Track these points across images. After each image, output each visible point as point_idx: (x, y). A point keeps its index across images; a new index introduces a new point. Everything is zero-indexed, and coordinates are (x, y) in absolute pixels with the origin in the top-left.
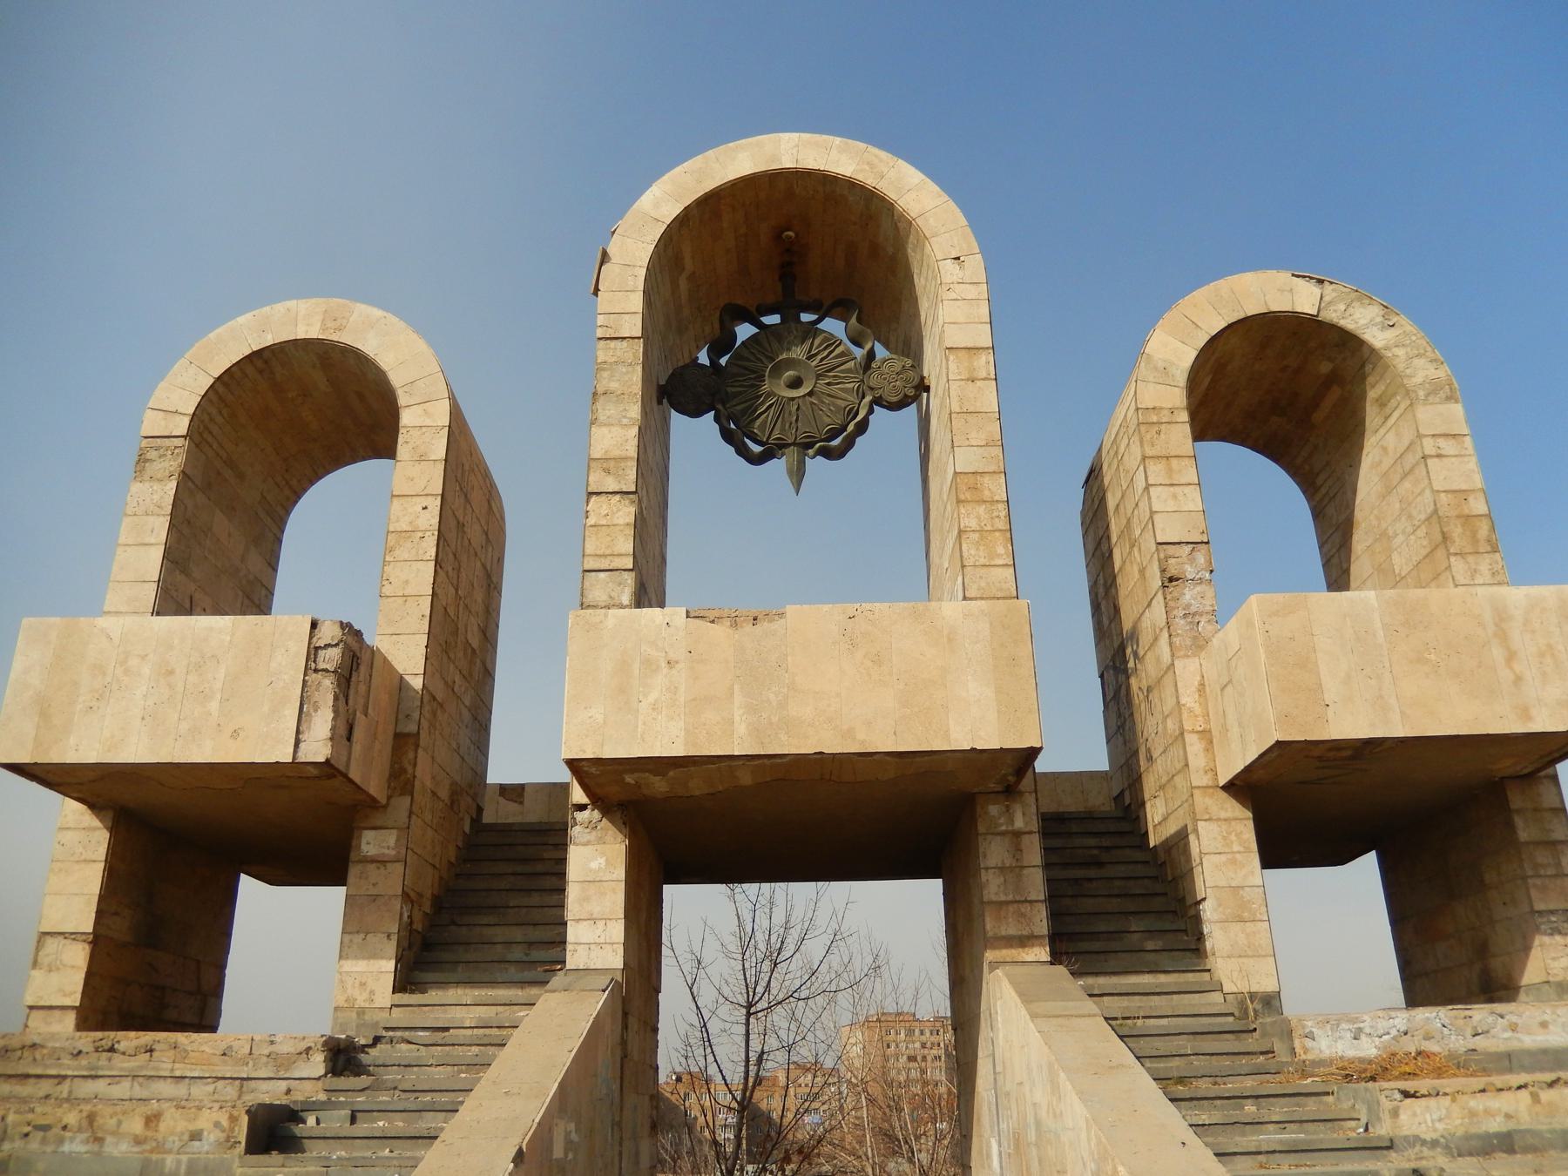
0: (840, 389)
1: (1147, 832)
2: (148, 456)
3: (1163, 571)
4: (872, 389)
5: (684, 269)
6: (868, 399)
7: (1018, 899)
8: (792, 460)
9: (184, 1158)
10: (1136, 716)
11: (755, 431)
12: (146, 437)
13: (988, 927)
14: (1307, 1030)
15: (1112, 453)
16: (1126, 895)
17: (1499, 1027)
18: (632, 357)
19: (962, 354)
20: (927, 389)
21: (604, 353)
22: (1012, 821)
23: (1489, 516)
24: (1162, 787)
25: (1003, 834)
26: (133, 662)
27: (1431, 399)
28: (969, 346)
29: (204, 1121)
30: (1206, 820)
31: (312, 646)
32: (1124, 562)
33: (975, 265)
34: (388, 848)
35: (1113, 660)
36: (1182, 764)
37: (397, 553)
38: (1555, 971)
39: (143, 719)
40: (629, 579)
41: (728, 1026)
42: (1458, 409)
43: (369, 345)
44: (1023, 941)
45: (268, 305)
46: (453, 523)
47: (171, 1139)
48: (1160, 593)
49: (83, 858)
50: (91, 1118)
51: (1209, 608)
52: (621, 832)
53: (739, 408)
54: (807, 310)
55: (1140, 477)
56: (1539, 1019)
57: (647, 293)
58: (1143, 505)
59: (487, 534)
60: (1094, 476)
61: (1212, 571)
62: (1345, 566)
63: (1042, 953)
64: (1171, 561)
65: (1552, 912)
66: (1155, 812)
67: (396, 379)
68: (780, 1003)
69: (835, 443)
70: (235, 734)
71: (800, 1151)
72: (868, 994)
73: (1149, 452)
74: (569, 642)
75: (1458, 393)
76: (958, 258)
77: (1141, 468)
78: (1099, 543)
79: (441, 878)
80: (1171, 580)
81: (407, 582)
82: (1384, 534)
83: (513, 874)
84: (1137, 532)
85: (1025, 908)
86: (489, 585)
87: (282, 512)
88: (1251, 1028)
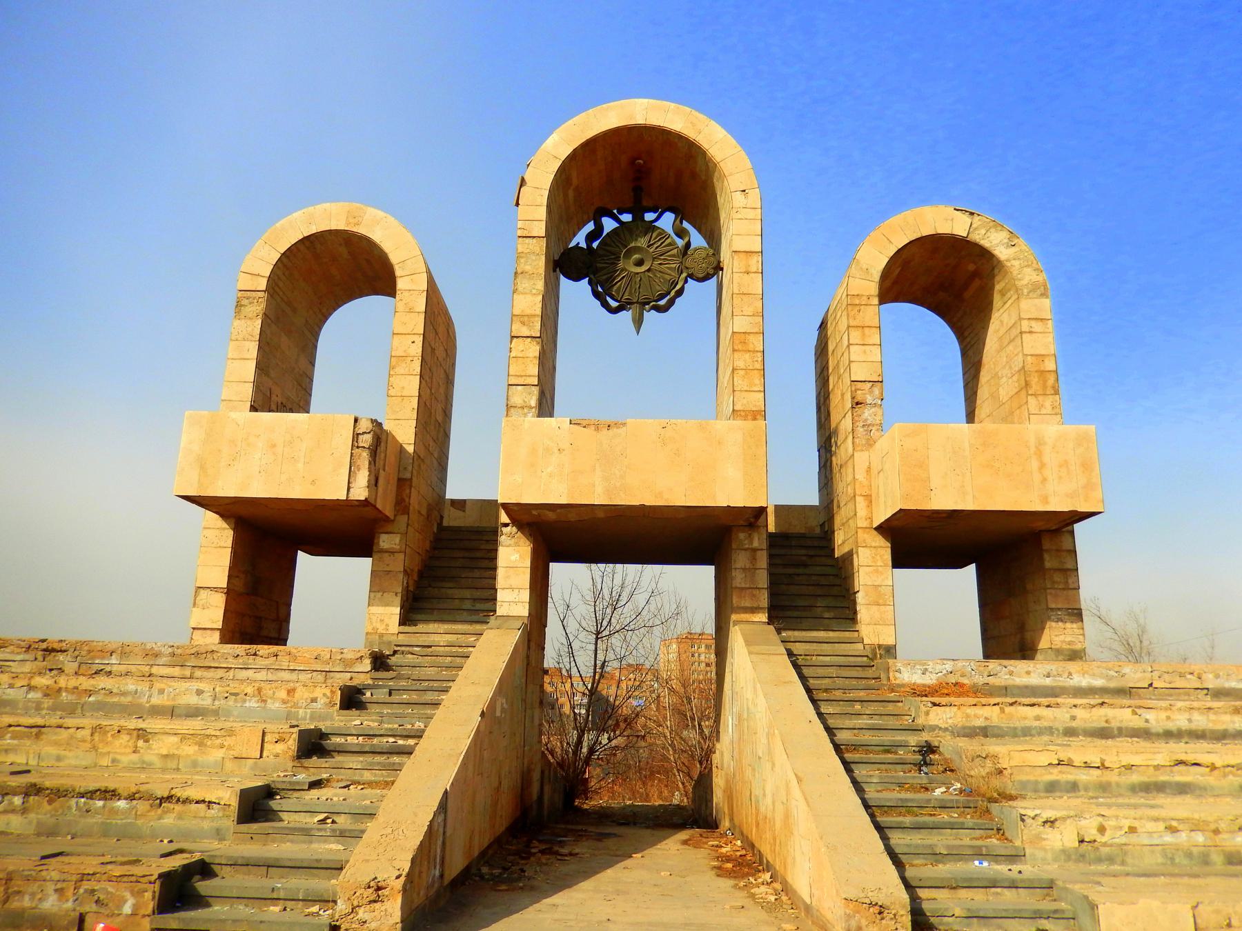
0: (667, 268)
1: (834, 549)
2: (243, 303)
3: (853, 398)
6: (684, 275)
7: (752, 586)
9: (309, 711)
10: (834, 480)
11: (613, 293)
12: (240, 291)
13: (734, 602)
14: (897, 668)
15: (833, 317)
16: (818, 585)
17: (1002, 673)
18: (539, 250)
19: (742, 255)
20: (722, 269)
21: (522, 246)
22: (751, 542)
24: (843, 524)
25: (746, 550)
28: (747, 250)
29: (318, 693)
30: (863, 547)
32: (834, 386)
33: (755, 197)
34: (395, 544)
38: (1056, 642)
40: (536, 390)
41: (584, 645)
42: (1047, 303)
43: (377, 236)
44: (753, 610)
45: (313, 206)
46: (430, 349)
47: (301, 701)
49: (218, 545)
50: (259, 690)
54: (649, 211)
55: (845, 337)
56: (1026, 670)
57: (548, 206)
58: (846, 355)
59: (447, 351)
60: (823, 326)
61: (882, 399)
62: (975, 389)
63: (763, 617)
64: (859, 392)
65: (1059, 609)
66: (839, 537)
67: (394, 258)
68: (618, 632)
69: (662, 302)
70: (313, 482)
71: (625, 720)
72: (672, 627)
73: (852, 324)
76: (744, 191)
77: (847, 333)
79: (422, 559)
80: (857, 404)
82: (996, 374)
83: (463, 558)
84: (842, 371)
85: (756, 592)
86: (448, 382)
87: (317, 329)
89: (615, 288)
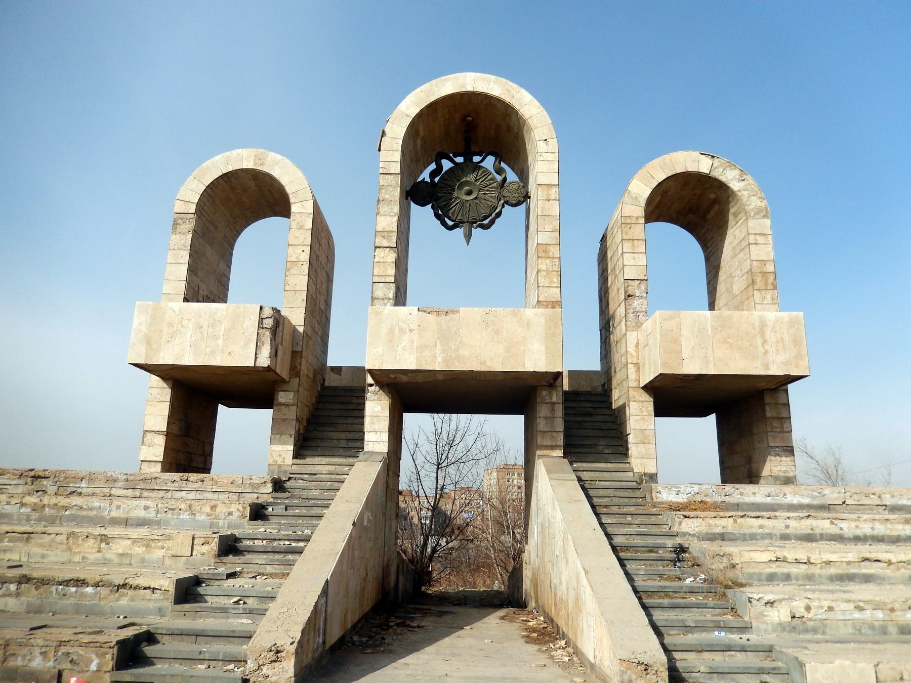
0: (489, 196)
2: (178, 222)
3: (626, 292)
4: (504, 197)
5: (419, 135)
6: (502, 202)
7: (552, 430)
8: (466, 229)
9: (226, 521)
10: (612, 352)
11: (450, 215)
13: (538, 441)
16: (600, 429)
19: (544, 187)
20: (529, 197)
21: (383, 181)
23: (775, 273)
24: (618, 385)
26: (185, 322)
27: (756, 216)
29: (233, 508)
31: (260, 317)
32: (612, 283)
33: (553, 143)
34: (290, 399)
35: (605, 325)
36: (626, 377)
37: (291, 271)
38: (774, 471)
39: (191, 346)
40: (393, 286)
41: (428, 473)
42: (768, 222)
43: (276, 173)
44: (552, 448)
46: (315, 256)
48: (623, 302)
50: (190, 506)
51: (644, 310)
52: (387, 396)
53: (443, 203)
56: (752, 492)
58: (620, 260)
59: (328, 258)
60: (604, 239)
61: (647, 293)
62: (715, 286)
63: (560, 453)
64: (630, 288)
65: (777, 447)
66: (615, 394)
67: (289, 190)
68: (453, 463)
69: (486, 222)
70: (230, 354)
71: (459, 528)
72: (493, 460)
73: (625, 237)
74: (368, 320)
75: (769, 213)
76: (546, 140)
77: (621, 244)
78: (603, 271)
79: (310, 410)
80: (629, 296)
81: (296, 285)
85: (555, 434)
87: (233, 242)
88: (639, 488)
89: (451, 211)
